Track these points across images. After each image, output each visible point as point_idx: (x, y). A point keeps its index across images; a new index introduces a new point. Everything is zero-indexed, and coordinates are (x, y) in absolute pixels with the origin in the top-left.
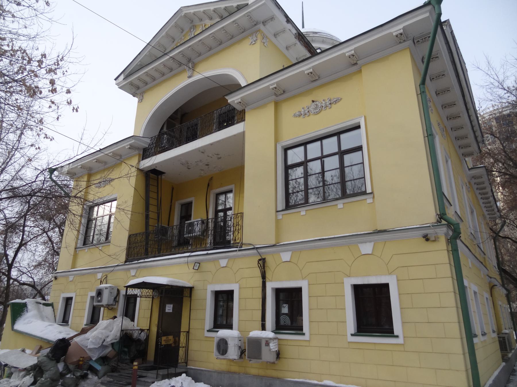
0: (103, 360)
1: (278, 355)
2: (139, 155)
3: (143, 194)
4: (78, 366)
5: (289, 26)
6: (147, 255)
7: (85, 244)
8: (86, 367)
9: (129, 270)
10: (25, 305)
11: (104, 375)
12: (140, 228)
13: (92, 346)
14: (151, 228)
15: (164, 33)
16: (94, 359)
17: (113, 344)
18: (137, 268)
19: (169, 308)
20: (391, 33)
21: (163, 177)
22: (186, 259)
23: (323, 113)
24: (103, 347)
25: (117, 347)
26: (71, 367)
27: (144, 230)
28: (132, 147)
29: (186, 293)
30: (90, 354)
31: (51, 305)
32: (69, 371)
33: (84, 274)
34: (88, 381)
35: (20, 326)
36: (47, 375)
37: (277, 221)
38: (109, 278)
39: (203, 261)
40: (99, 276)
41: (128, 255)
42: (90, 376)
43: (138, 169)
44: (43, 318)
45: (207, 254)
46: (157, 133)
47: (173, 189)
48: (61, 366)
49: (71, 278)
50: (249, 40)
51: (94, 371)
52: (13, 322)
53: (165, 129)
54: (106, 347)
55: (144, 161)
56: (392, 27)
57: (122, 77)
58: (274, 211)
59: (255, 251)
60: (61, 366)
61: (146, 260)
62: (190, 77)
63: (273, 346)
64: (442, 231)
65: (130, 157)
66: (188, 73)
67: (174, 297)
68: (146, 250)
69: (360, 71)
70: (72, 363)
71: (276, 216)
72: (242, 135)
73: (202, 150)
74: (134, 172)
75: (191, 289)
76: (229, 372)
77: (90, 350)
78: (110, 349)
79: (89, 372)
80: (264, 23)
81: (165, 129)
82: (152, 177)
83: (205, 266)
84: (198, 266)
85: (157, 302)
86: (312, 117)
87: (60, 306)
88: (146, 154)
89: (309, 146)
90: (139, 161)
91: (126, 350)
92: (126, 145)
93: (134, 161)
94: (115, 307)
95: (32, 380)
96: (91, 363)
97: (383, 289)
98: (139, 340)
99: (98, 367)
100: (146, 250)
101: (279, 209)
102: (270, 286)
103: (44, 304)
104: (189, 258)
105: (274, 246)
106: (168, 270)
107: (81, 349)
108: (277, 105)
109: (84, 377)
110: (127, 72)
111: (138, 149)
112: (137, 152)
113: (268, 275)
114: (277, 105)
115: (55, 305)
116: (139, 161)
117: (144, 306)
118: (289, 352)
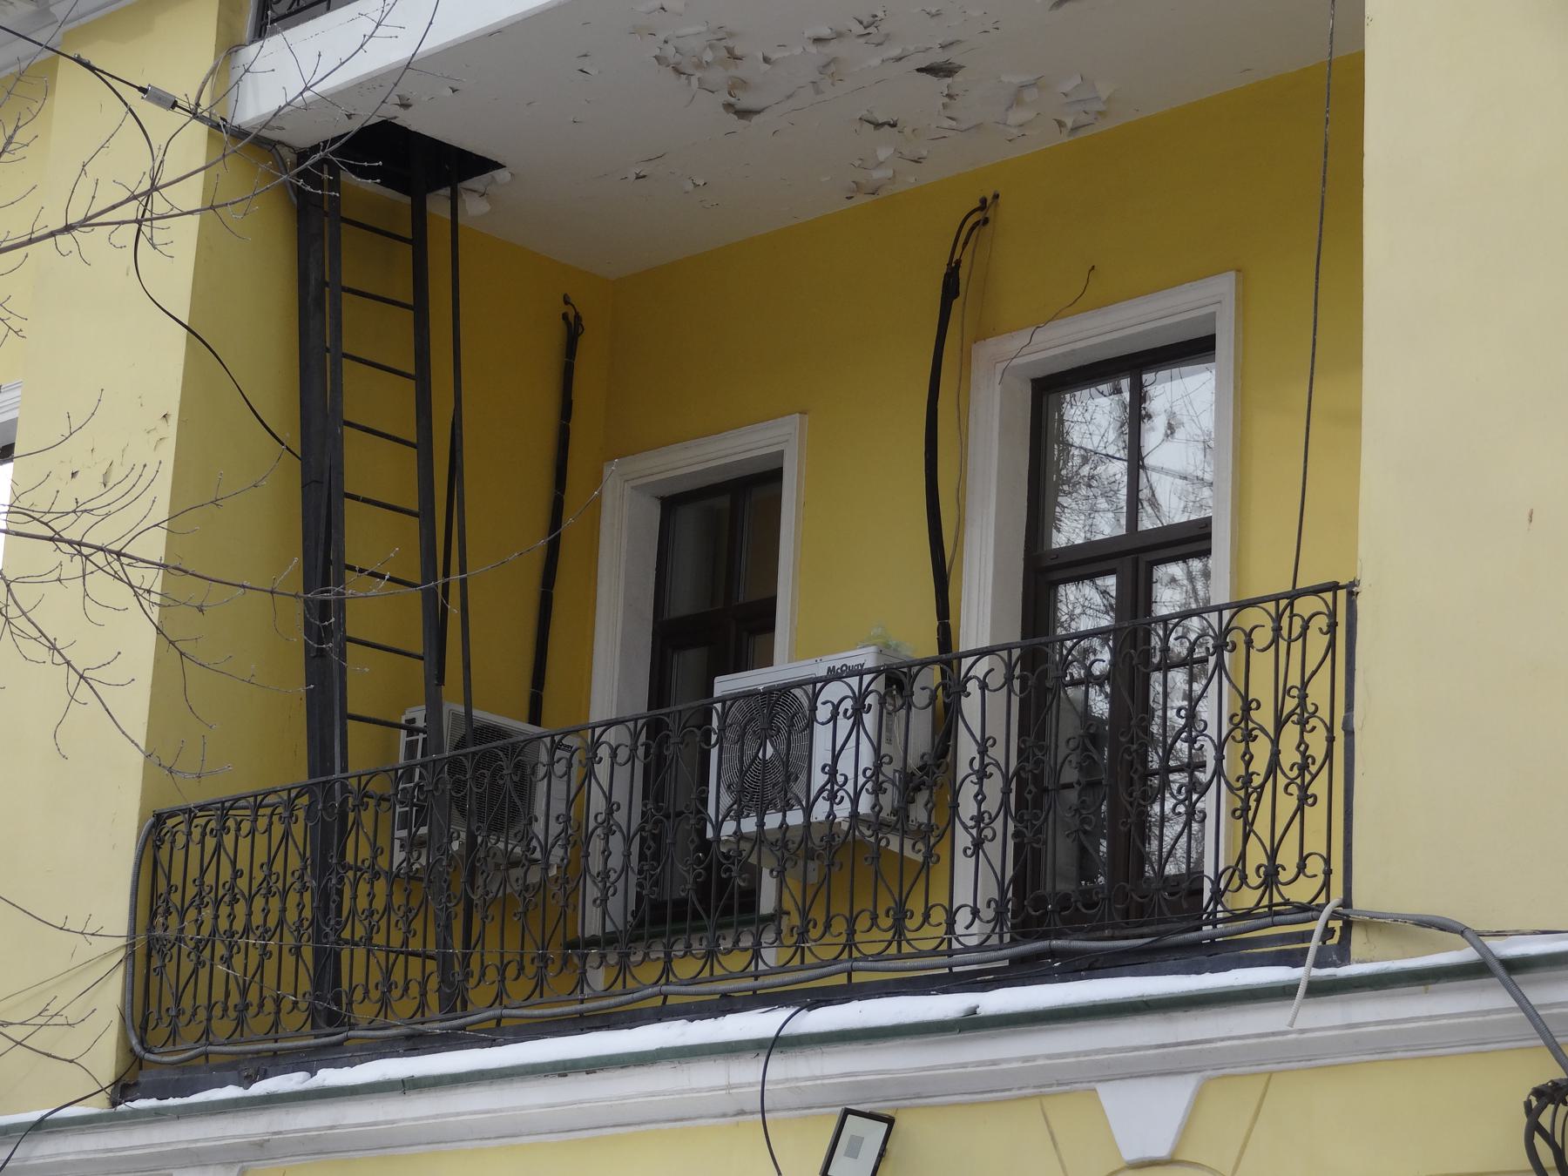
12: (259, 750)
14: (363, 750)
22: (746, 1072)
27: (300, 774)
39: (920, 1091)
41: (142, 1018)
43: (216, 126)
45: (972, 1024)
55: (273, 43)
59: (1489, 999)
61: (329, 1077)
104: (783, 1068)
116: (229, 49)
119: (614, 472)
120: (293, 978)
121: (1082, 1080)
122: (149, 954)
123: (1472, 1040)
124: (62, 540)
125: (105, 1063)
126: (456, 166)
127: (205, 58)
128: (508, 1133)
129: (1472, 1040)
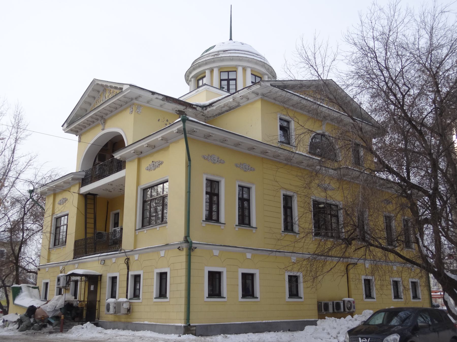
0: (57, 318)
1: (129, 310)
2: (79, 183)
3: (83, 212)
4: (41, 320)
5: (156, 96)
6: (86, 253)
7: (55, 245)
8: (46, 321)
9: (74, 264)
10: (20, 288)
11: (56, 326)
12: (83, 237)
13: (49, 310)
14: (88, 236)
15: (87, 96)
16: (50, 317)
17: (61, 309)
18: (78, 263)
19: (92, 288)
20: (173, 131)
21: (98, 196)
22: (97, 258)
23: (157, 169)
24: (55, 310)
25: (63, 310)
26: (37, 320)
27: (84, 238)
28: (73, 179)
29: (99, 278)
30: (48, 314)
31: (38, 288)
32: (36, 323)
33: (53, 267)
34: (47, 328)
35: (17, 301)
36: (24, 323)
37: (136, 236)
38: (66, 269)
39: (106, 259)
40: (61, 268)
41: (75, 254)
42: (48, 326)
43: (79, 194)
44: (31, 296)
45: (107, 255)
46: (91, 167)
47: (108, 203)
48: (32, 320)
49: (47, 269)
50: (129, 110)
51: (50, 323)
52: (14, 299)
53: (97, 161)
54: (57, 310)
55: (83, 188)
56: (173, 128)
57: (66, 125)
58: (134, 230)
59: (124, 254)
60: (32, 320)
61: (83, 258)
62: (103, 130)
63: (126, 306)
64: (185, 246)
65: (74, 185)
66: (101, 127)
67: (94, 280)
68: (86, 251)
69: (168, 147)
70: (38, 319)
71: (135, 233)
72: (123, 179)
73: (111, 184)
74: (76, 196)
75: (101, 276)
76: (114, 321)
77: (49, 312)
78: (59, 312)
79: (48, 324)
80: (136, 98)
81: (97, 161)
82: (89, 199)
83: (107, 262)
84: (104, 262)
85: (87, 284)
86: (153, 171)
87: (42, 288)
88: (84, 182)
89: (165, 184)
90: (79, 188)
91: (69, 312)
92: (69, 178)
93: (75, 189)
94: (68, 288)
95: (18, 326)
96: (49, 319)
97: (219, 274)
98: (77, 308)
99: (53, 321)
100: (86, 251)
101: (137, 228)
102: (130, 273)
103: (33, 287)
104: (100, 258)
105: (132, 251)
106: (91, 265)
107: (43, 311)
108: (139, 160)
109: (45, 326)
110: (69, 121)
111: (78, 179)
112: (77, 182)
113: (130, 268)
114: (139, 160)
115: (40, 287)
116: (79, 188)
117: (82, 286)
118: (136, 308)
119: (111, 213)
120: (84, 250)
121: (111, 258)
122: (75, 250)
123: (122, 256)
124: (319, 75)
125: (73, 258)
126: (96, 195)
127: (78, 189)
128: (90, 261)
129: (122, 256)
